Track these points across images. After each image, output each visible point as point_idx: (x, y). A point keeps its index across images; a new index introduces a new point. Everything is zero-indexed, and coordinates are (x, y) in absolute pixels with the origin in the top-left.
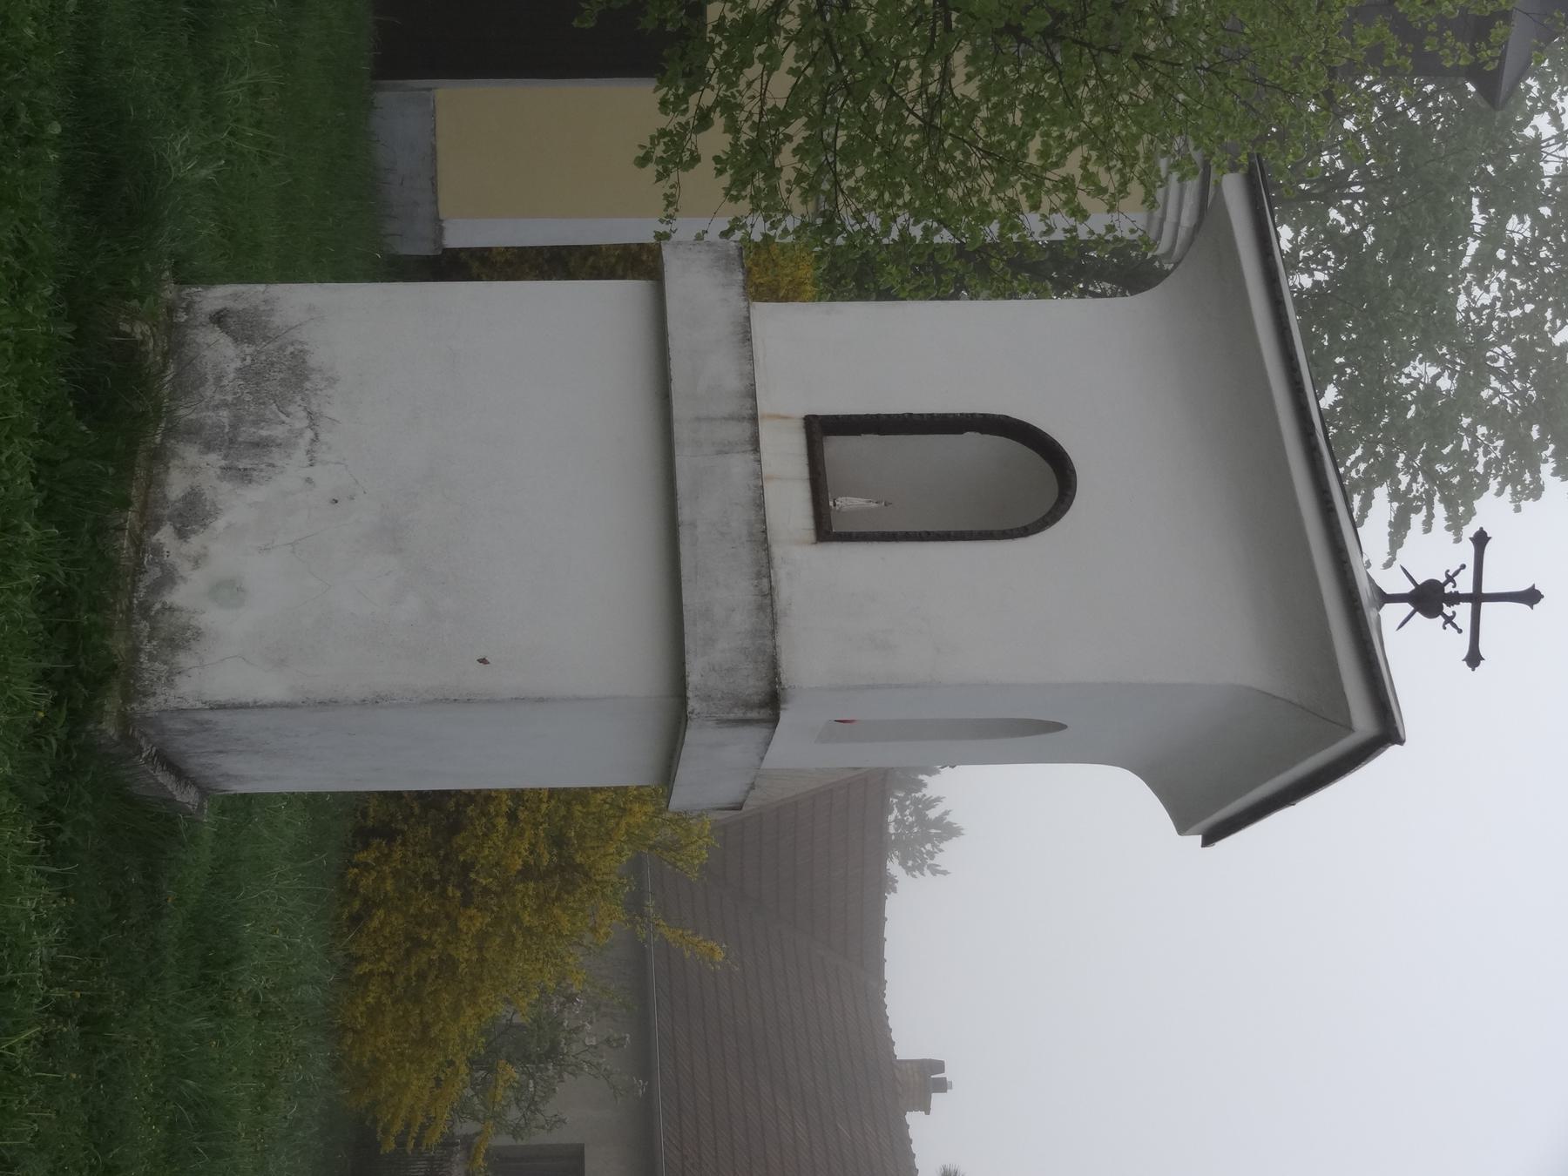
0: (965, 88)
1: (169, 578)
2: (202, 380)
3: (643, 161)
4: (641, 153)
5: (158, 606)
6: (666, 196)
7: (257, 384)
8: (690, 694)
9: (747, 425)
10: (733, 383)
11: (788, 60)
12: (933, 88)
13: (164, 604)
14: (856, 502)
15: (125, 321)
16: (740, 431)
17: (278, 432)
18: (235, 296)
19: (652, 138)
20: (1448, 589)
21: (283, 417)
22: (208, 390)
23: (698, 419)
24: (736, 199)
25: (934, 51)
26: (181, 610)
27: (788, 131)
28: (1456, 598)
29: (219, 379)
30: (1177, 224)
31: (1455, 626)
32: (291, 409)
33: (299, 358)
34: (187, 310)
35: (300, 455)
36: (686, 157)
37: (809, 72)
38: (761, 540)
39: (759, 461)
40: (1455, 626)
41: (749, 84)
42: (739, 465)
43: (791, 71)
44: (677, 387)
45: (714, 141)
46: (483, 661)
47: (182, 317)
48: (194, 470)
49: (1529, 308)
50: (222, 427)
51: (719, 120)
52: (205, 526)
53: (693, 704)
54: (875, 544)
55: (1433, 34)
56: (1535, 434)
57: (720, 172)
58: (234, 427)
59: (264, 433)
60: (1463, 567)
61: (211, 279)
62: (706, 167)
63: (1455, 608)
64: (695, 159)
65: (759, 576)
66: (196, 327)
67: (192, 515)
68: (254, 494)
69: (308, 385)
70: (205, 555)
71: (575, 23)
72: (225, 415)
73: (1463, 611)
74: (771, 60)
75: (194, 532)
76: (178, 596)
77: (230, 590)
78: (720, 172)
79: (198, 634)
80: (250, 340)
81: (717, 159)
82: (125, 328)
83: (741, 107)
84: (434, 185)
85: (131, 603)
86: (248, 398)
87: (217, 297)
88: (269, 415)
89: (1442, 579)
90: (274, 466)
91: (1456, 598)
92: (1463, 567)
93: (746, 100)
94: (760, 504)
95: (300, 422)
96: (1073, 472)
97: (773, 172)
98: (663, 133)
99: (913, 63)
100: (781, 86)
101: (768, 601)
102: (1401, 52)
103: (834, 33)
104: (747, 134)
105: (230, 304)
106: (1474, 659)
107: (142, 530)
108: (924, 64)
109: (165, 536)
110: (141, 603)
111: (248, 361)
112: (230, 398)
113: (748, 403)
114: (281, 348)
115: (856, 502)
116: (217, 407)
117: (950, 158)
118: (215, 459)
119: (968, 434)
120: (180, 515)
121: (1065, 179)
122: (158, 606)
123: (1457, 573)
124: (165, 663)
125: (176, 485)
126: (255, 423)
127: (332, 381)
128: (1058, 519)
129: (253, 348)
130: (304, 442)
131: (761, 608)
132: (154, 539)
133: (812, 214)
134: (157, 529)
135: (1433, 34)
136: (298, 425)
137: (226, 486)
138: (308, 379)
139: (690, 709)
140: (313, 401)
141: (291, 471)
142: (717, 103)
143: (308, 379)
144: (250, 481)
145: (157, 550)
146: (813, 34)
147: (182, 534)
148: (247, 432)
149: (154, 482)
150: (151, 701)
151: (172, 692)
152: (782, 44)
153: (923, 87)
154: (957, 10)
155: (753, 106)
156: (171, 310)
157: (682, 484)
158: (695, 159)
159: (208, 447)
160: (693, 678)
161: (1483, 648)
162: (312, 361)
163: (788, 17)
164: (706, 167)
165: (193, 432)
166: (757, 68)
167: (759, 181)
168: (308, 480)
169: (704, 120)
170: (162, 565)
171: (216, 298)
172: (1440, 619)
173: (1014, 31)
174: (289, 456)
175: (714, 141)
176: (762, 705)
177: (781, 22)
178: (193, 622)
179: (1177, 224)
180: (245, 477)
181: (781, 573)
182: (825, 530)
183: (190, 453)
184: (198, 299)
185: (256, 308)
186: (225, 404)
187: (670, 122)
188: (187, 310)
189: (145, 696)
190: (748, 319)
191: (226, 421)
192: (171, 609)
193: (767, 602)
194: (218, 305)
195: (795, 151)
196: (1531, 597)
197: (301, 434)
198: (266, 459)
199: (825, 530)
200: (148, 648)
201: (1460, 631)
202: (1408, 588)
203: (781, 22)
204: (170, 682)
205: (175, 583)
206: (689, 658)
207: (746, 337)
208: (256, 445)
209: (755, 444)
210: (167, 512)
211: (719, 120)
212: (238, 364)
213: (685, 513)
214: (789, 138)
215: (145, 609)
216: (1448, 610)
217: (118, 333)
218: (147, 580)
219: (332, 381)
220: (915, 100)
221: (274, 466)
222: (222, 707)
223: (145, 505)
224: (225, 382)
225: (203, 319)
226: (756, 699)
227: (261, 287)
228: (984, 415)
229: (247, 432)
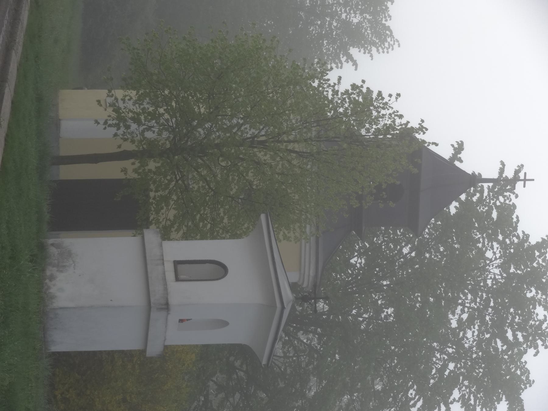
1: (49, 288)
21: (68, 261)
30: (309, 275)
38: (164, 279)
39: (164, 267)
44: (148, 255)
46: (111, 300)
53: (152, 305)
54: (188, 282)
59: (64, 264)
67: (52, 278)
72: (56, 261)
76: (51, 291)
87: (51, 241)
96: (228, 273)
111: (59, 252)
112: (57, 258)
119: (207, 264)
122: (48, 292)
125: (48, 273)
128: (224, 277)
132: (45, 282)
133: (157, 125)
147: (51, 281)
157: (149, 270)
160: (152, 300)
168: (74, 272)
179: (309, 275)
180: (62, 272)
182: (177, 279)
193: (166, 289)
199: (177, 279)
209: (163, 264)
212: (57, 252)
213: (150, 275)
222: (61, 308)
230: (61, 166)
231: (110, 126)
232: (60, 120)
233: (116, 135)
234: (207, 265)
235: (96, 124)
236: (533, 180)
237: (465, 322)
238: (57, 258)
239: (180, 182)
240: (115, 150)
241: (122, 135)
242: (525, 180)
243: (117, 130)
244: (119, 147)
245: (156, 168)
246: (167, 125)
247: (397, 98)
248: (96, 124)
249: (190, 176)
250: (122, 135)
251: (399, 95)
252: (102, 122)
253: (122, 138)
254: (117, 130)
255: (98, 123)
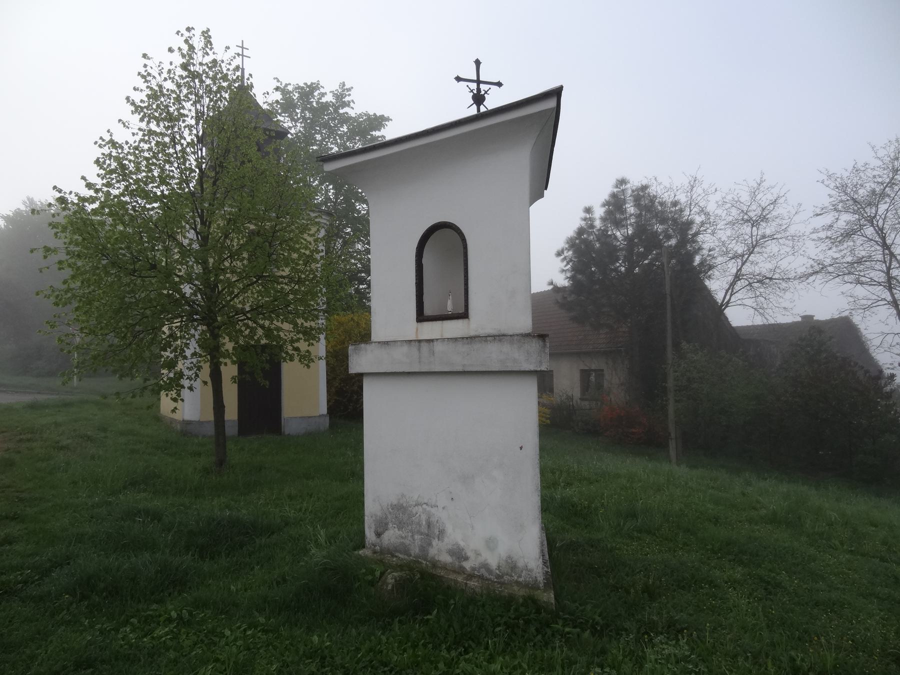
0: (287, 271)
1: (485, 566)
2: (403, 544)
3: (308, 367)
4: (306, 367)
5: (497, 571)
6: (319, 360)
7: (404, 523)
8: (539, 369)
9: (422, 344)
10: (405, 349)
11: (279, 324)
12: (286, 281)
13: (496, 569)
14: (449, 303)
15: (387, 586)
16: (425, 347)
17: (424, 518)
18: (370, 528)
19: (301, 364)
20: (475, 92)
21: (418, 515)
22: (407, 542)
23: (420, 362)
24: (319, 339)
25: (276, 280)
26: (499, 563)
27: (300, 324)
28: (479, 90)
29: (402, 537)
31: (488, 90)
32: (414, 512)
33: (393, 507)
34: (375, 546)
35: (433, 510)
36: (307, 354)
37: (282, 317)
40: (488, 90)
41: (286, 335)
42: (439, 347)
43: (282, 323)
45: (303, 346)
46: (521, 448)
47: (378, 548)
48: (439, 551)
49: (337, 138)
50: (422, 539)
51: (296, 345)
52: (463, 549)
55: (270, 133)
56: (369, 137)
57: (313, 344)
58: (422, 534)
59: (424, 523)
60: (468, 86)
61: (362, 533)
62: (311, 349)
63: (482, 90)
64: (308, 351)
65: (486, 341)
66: (382, 543)
67: (459, 554)
68: (449, 529)
69: (404, 505)
70: (475, 551)
71: (267, 387)
73: (483, 87)
74: (279, 329)
75: (466, 554)
77: (491, 543)
78: (313, 344)
79: (509, 557)
80: (387, 524)
81: (309, 345)
82: (390, 587)
83: (292, 337)
84: (309, 417)
85: (496, 582)
86: (410, 527)
87: (370, 535)
88: (417, 520)
89: (472, 94)
90: (438, 521)
91: (479, 90)
92: (468, 86)
93: (290, 337)
94: (455, 340)
95: (419, 509)
96: (439, 223)
97: (311, 328)
98: (300, 361)
99: (279, 287)
100: (287, 326)
101: (497, 338)
102: (275, 143)
103: (269, 310)
104: (301, 336)
105: (373, 530)
106: (499, 84)
107: (465, 574)
108: (278, 283)
109: (467, 565)
110: (496, 578)
111: (395, 526)
112: (410, 534)
113: (413, 343)
114: (390, 513)
115: (449, 303)
116: (414, 540)
117: (308, 276)
118: (435, 542)
120: (458, 558)
121: (315, 242)
122: (497, 571)
123: (470, 89)
124: (522, 571)
125: (446, 558)
126: (420, 526)
127: (403, 496)
129: (390, 524)
130: (428, 509)
131: (500, 341)
134: (465, 568)
135: (270, 133)
136: (421, 510)
137: (446, 540)
138: (402, 504)
139: (546, 370)
140: (411, 503)
141: (439, 514)
142: (291, 345)
143: (402, 504)
144: (444, 530)
145: (473, 569)
146: (270, 316)
147: (466, 559)
148: (424, 529)
149: (444, 567)
150: (539, 579)
151: (535, 570)
152: (274, 326)
153: (286, 284)
154: (263, 273)
155: (292, 335)
156: (375, 552)
158: (308, 351)
159: (430, 544)
160: (532, 367)
161: (496, 81)
162: (395, 502)
163: (265, 324)
164: (311, 349)
165: (424, 549)
166: (282, 334)
167: (314, 332)
169: (297, 349)
170: (480, 568)
171: (370, 535)
172: (486, 95)
173: (270, 255)
174: (434, 514)
175: (303, 346)
176: (544, 341)
177: (267, 326)
178: (504, 559)
180: (442, 532)
181: (481, 332)
182: (464, 315)
183: (432, 552)
184: (371, 542)
185: (374, 520)
186: (412, 536)
187: (297, 359)
188: (375, 546)
189: (537, 581)
190: (379, 342)
191: (419, 537)
192: (499, 567)
193: (499, 337)
194: (373, 535)
195: (306, 322)
196: (478, 63)
197: (424, 510)
198: (435, 523)
199: (464, 315)
200: (516, 578)
201: (490, 88)
202: (475, 106)
203: (267, 326)
204: (531, 570)
205: (488, 564)
206: (522, 369)
207: (386, 343)
208: (429, 526)
210: (457, 563)
211: (296, 345)
212: (396, 530)
213: (459, 368)
214: (302, 324)
215: (498, 577)
216: (483, 93)
217: (392, 590)
218: (486, 575)
219: (403, 496)
220: (291, 286)
221: (438, 521)
223: (454, 572)
224: (403, 535)
225: (378, 540)
226: (541, 343)
227: (366, 518)
228: (416, 256)
229: (424, 529)
230: (225, 419)
231: (179, 395)
232: (183, 421)
233: (191, 388)
234: (424, 261)
235: (177, 411)
236: (243, 41)
237: (346, 119)
238: (410, 534)
239: (249, 315)
240: (209, 388)
241: (190, 380)
242: (242, 47)
243: (184, 388)
244: (205, 383)
245: (230, 341)
246: (888, 264)
247: (149, 59)
248: (177, 411)
249: (240, 306)
250: (190, 380)
251: (145, 56)
252: (175, 404)
253: (195, 380)
254: (184, 388)
255: (176, 408)
